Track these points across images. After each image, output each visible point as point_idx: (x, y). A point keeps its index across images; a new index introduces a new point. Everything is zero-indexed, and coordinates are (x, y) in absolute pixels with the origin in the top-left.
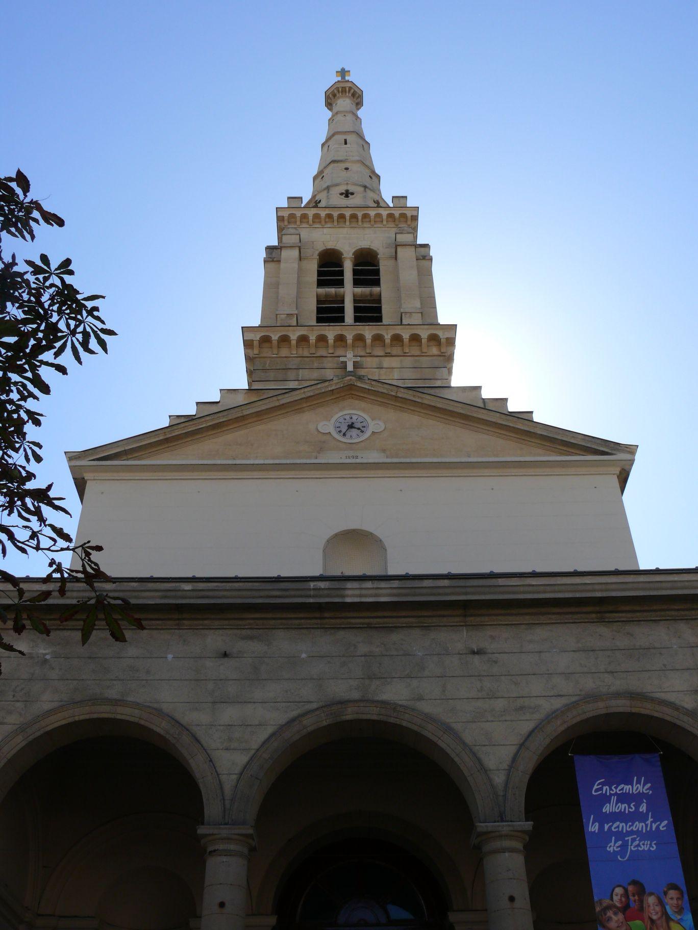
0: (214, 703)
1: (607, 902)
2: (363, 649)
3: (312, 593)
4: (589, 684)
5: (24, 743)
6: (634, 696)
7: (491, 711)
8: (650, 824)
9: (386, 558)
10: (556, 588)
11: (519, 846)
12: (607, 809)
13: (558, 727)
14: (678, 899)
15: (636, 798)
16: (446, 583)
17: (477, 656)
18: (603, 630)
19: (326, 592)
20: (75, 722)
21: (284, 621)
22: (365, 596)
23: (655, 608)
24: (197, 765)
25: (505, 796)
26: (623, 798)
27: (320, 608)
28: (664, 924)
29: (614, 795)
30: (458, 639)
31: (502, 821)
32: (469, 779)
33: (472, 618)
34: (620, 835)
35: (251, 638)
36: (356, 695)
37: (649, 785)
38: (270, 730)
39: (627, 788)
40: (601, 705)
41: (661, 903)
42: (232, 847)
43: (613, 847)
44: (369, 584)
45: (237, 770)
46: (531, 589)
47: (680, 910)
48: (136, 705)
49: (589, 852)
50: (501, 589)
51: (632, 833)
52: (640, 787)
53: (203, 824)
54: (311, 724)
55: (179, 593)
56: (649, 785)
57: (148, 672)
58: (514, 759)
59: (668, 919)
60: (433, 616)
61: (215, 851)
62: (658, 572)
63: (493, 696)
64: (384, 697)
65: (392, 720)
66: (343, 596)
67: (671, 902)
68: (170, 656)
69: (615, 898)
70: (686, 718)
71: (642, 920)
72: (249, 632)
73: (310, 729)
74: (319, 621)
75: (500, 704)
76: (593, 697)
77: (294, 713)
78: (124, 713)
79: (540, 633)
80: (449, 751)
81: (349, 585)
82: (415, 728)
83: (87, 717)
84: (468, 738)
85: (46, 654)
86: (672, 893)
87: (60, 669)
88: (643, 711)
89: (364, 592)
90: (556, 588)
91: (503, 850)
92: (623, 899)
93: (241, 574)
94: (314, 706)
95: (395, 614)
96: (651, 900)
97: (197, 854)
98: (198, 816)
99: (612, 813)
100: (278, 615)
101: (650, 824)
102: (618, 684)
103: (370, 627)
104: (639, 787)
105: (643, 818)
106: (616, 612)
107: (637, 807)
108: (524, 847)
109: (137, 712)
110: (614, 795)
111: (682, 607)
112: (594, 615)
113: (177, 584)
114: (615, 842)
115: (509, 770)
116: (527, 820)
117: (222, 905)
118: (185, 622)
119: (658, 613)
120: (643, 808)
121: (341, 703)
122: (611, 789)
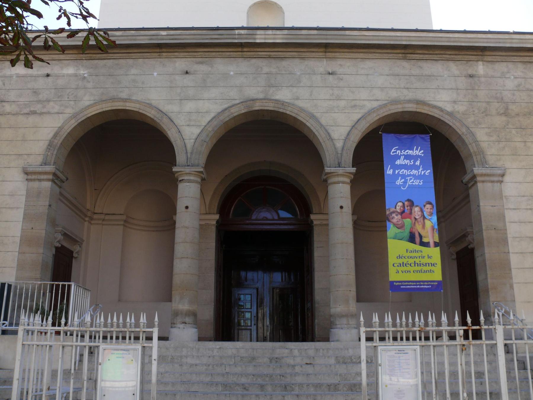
0: (181, 100)
1: (393, 209)
2: (266, 70)
3: (237, 37)
4: (394, 94)
5: (76, 124)
6: (418, 102)
7: (337, 107)
8: (421, 171)
9: (284, 18)
10: (380, 38)
11: (348, 180)
12: (398, 162)
13: (374, 118)
14: (431, 209)
15: (416, 158)
16: (315, 32)
17: (331, 76)
18: (405, 63)
19: (244, 36)
20: (103, 112)
21: (220, 53)
22: (268, 39)
23: (436, 52)
24: (172, 134)
25: (342, 154)
26: (407, 157)
27: (241, 45)
28: (422, 221)
29: (403, 155)
30: (319, 65)
31: (339, 167)
32: (322, 144)
33: (330, 54)
34: (404, 176)
35: (201, 63)
36: (261, 96)
37: (422, 151)
38: (212, 115)
39: (410, 152)
40: (400, 106)
41: (422, 211)
42: (192, 178)
43: (399, 182)
44: (270, 32)
45: (194, 137)
46: (365, 37)
47: (431, 214)
48: (137, 102)
49: (386, 184)
50: (347, 37)
51: (410, 175)
52: (417, 152)
53: (176, 166)
54: (236, 111)
55: (159, 37)
56: (422, 151)
57: (143, 83)
58: (348, 134)
59: (424, 218)
60: (307, 52)
61: (182, 180)
62: (441, 31)
63: (339, 99)
64: (277, 97)
65: (281, 110)
66: (255, 39)
67: (427, 210)
68: (155, 74)
69: (397, 207)
70: (446, 116)
71: (411, 218)
72: (200, 60)
73: (235, 114)
74: (240, 53)
75: (342, 103)
76: (395, 102)
77: (226, 106)
78: (130, 106)
79: (369, 64)
80: (312, 128)
81: (259, 32)
82: (294, 115)
83: (110, 109)
84: (323, 121)
85: (84, 74)
86: (428, 206)
87: (93, 82)
88: (423, 111)
89: (267, 37)
90: (380, 38)
91: (338, 183)
92: (402, 208)
93: (196, 26)
94: (238, 102)
95: (285, 50)
96: (417, 209)
97: (173, 182)
98: (173, 161)
99: (401, 165)
100: (217, 50)
101: (421, 171)
102: (410, 95)
103: (270, 57)
104: (417, 152)
105: (417, 168)
106: (414, 54)
107: (415, 162)
108: (351, 181)
109: (138, 106)
110: (403, 155)
111: (453, 53)
112: (400, 55)
113: (158, 32)
114: (401, 180)
115: (345, 140)
116: (353, 167)
117: (187, 207)
118: (164, 54)
119: (439, 56)
120: (418, 163)
121: (253, 100)
122: (401, 152)
